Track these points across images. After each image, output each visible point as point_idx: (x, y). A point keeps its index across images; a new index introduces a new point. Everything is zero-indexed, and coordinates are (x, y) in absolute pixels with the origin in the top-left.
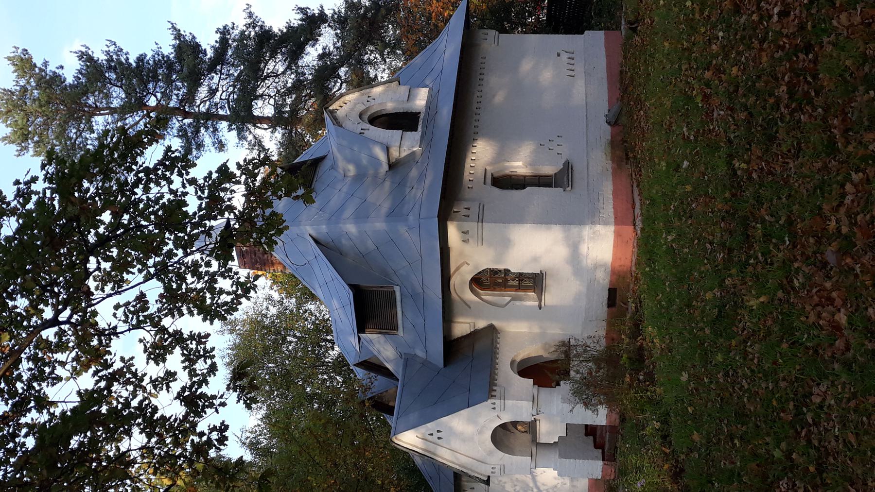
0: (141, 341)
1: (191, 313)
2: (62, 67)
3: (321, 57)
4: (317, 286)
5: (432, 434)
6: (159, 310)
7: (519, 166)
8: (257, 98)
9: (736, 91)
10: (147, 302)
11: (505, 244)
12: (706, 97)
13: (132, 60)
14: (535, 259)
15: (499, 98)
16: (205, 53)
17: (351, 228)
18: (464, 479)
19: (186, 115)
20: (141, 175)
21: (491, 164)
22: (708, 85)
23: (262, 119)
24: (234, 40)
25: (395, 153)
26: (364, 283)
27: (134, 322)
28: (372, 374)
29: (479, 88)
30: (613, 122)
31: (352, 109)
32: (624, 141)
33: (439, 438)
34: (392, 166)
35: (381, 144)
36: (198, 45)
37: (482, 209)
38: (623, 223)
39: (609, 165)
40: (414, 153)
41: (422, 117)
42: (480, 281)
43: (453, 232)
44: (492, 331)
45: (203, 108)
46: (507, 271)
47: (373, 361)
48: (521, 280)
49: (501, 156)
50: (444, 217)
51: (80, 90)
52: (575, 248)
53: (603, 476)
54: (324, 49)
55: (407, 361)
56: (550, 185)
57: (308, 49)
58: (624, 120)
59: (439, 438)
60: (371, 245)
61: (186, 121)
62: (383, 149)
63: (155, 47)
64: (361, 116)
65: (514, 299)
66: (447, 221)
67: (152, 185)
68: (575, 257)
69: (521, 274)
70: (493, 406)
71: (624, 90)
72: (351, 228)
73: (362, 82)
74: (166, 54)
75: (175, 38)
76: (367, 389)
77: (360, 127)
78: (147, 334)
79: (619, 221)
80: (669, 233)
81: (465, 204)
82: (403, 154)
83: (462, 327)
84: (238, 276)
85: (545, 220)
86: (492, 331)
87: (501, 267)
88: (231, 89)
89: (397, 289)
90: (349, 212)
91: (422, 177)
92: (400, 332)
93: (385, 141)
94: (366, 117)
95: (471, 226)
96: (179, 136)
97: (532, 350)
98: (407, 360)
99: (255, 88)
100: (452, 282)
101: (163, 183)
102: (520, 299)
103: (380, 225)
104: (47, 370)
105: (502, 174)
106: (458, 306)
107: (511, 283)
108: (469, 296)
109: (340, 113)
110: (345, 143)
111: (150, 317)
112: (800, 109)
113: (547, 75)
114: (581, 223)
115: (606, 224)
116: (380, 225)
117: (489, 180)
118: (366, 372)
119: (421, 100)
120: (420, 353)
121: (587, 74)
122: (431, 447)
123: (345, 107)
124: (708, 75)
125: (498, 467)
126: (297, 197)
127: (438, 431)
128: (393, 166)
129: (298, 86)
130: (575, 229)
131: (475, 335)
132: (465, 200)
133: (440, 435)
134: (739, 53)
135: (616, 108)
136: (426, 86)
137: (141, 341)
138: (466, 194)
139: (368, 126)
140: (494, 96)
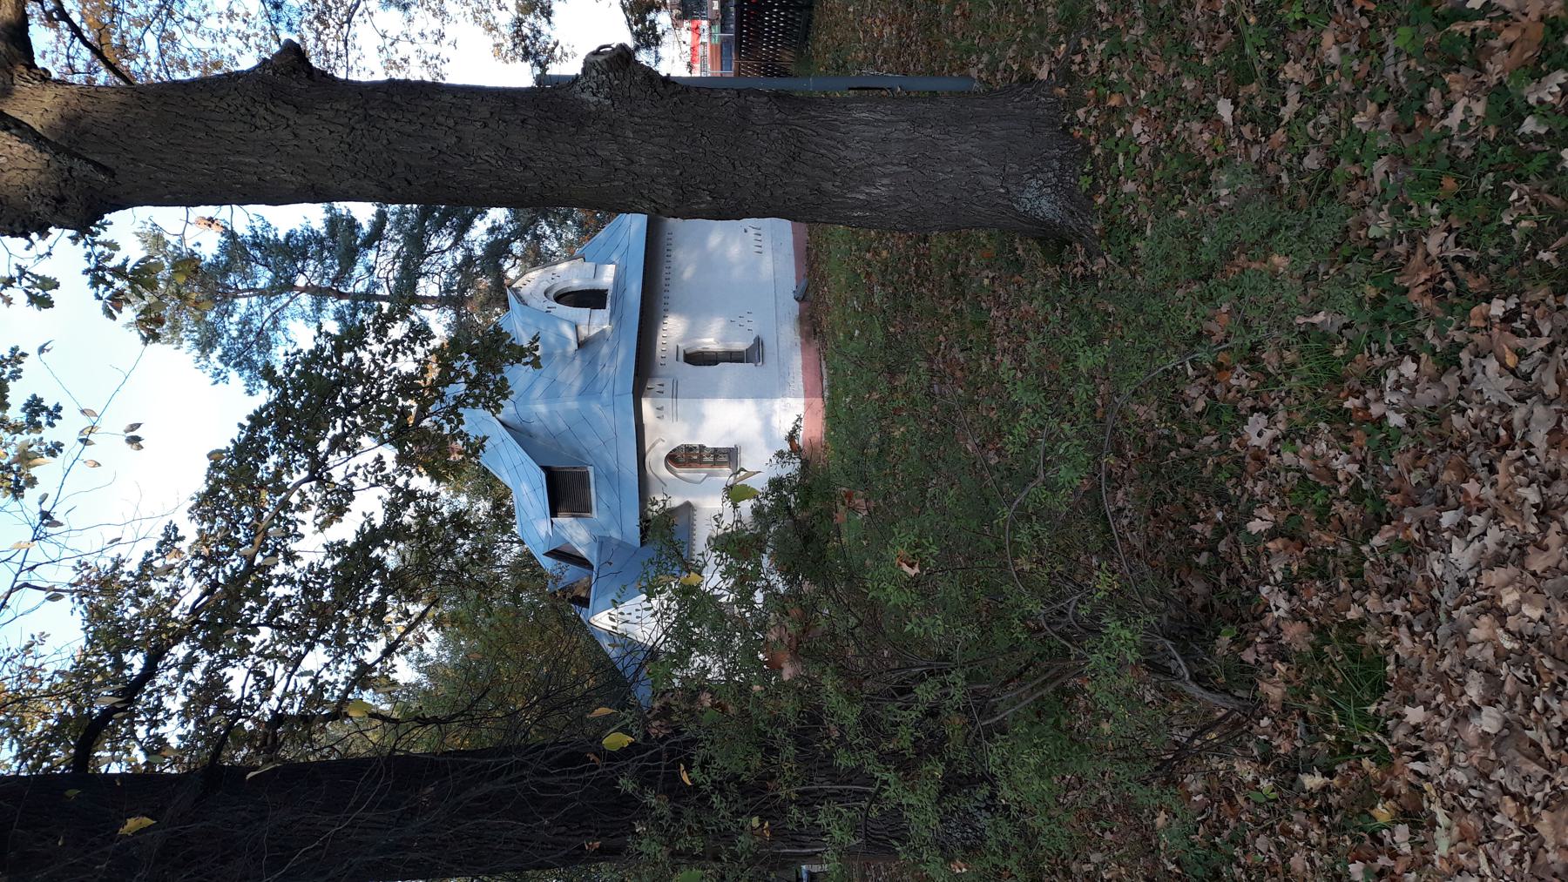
0: (380, 498)
1: (420, 475)
2: (199, 244)
3: (491, 231)
4: (503, 471)
6: (394, 471)
7: (710, 342)
8: (421, 275)
9: (886, 270)
10: (384, 463)
11: (699, 418)
12: (868, 275)
13: (282, 237)
14: (730, 433)
15: (688, 273)
16: (359, 226)
17: (541, 408)
19: (340, 296)
20: (390, 346)
21: (684, 340)
22: (869, 265)
23: (426, 300)
24: (393, 214)
25: (584, 332)
26: (554, 464)
27: (373, 481)
28: (563, 564)
29: (668, 265)
30: (801, 298)
31: (536, 287)
32: (811, 317)
35: (569, 322)
36: (353, 219)
37: (676, 384)
39: (798, 339)
40: (603, 331)
41: (609, 294)
42: (674, 459)
43: (647, 406)
44: (688, 507)
45: (361, 288)
46: (702, 447)
47: (568, 551)
48: (716, 456)
49: (692, 332)
50: (639, 392)
51: (221, 269)
54: (494, 222)
55: (601, 543)
56: (742, 361)
57: (476, 222)
58: (811, 295)
60: (562, 425)
61: (343, 302)
62: (571, 326)
63: (304, 222)
64: (546, 293)
65: (709, 475)
66: (793, 219)
67: (399, 355)
69: (716, 449)
71: (810, 266)
72: (541, 408)
73: (537, 258)
74: (315, 229)
75: (327, 212)
76: (558, 579)
77: (546, 305)
78: (384, 492)
79: (808, 394)
80: (847, 397)
81: (659, 381)
82: (593, 333)
85: (738, 394)
86: (688, 507)
87: (696, 443)
88: (390, 267)
89: (591, 470)
90: (539, 390)
91: (613, 354)
92: (595, 514)
93: (573, 319)
94: (551, 295)
95: (666, 402)
96: (336, 319)
98: (602, 543)
99: (417, 266)
101: (409, 353)
102: (717, 475)
103: (573, 404)
104: (291, 527)
105: (694, 350)
107: (706, 459)
108: (664, 472)
109: (524, 291)
110: (529, 321)
111: (387, 477)
112: (922, 284)
113: (735, 251)
114: (773, 396)
115: (796, 396)
116: (573, 404)
118: (555, 561)
119: (607, 276)
120: (615, 534)
121: (775, 250)
123: (530, 285)
124: (868, 256)
126: (527, 363)
128: (582, 344)
129: (469, 260)
130: (766, 403)
132: (661, 377)
134: (888, 239)
135: (803, 284)
136: (612, 263)
137: (380, 498)
138: (661, 371)
139: (555, 304)
140: (682, 273)
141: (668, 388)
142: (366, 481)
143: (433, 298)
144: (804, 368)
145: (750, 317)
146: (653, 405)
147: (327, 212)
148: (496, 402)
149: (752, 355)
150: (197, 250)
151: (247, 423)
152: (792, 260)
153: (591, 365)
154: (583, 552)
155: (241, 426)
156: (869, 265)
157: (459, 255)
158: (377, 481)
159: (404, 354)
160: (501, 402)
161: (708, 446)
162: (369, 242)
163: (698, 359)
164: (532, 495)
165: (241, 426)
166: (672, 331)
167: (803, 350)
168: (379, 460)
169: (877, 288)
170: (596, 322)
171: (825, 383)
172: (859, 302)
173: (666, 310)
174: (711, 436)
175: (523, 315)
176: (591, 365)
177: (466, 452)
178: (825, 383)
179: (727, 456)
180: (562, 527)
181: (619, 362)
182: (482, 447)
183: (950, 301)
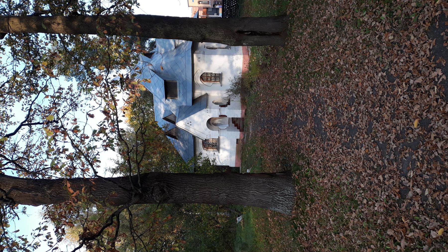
4: (151, 88)
5: (188, 123)
11: (210, 62)
18: (197, 138)
34: (176, 47)
38: (245, 55)
43: (195, 56)
44: (207, 95)
46: (211, 73)
50: (193, 53)
52: (231, 63)
53: (240, 138)
65: (213, 84)
68: (231, 66)
70: (207, 111)
83: (198, 93)
84: (51, 237)
86: (207, 95)
89: (178, 81)
95: (201, 56)
97: (219, 100)
100: (195, 77)
106: (196, 87)
115: (240, 54)
117: (206, 47)
122: (188, 128)
125: (208, 135)
130: (231, 57)
131: (201, 97)
133: (191, 123)
146: (197, 56)
174: (214, 69)
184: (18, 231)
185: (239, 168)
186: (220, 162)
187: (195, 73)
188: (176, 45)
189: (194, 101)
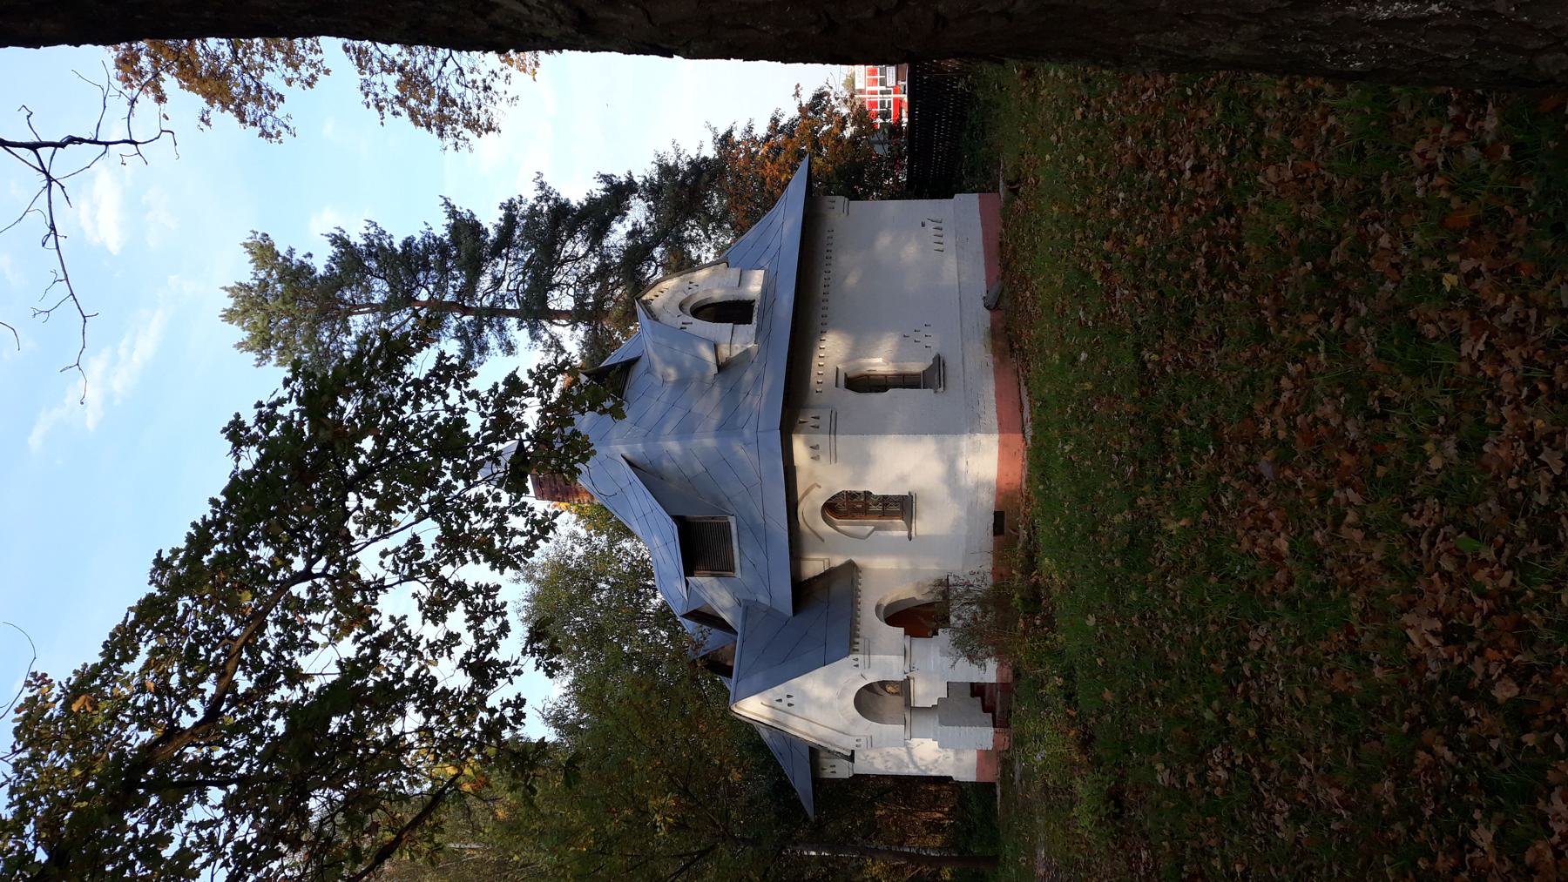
0: (415, 596)
2: (310, 255)
3: (631, 235)
6: (437, 557)
7: (879, 363)
8: (552, 287)
9: (1143, 265)
11: (864, 461)
14: (903, 479)
15: (852, 280)
16: (486, 232)
17: (673, 446)
18: (822, 754)
19: (465, 311)
20: (409, 389)
23: (560, 314)
24: (523, 217)
25: (725, 352)
26: (692, 514)
27: (406, 572)
29: (827, 268)
30: (993, 306)
31: (671, 299)
32: (1007, 329)
33: (790, 705)
36: (478, 225)
37: (834, 417)
40: (747, 351)
41: (756, 305)
44: (851, 567)
46: (868, 494)
50: (788, 428)
51: (333, 283)
54: (634, 225)
56: (918, 387)
57: (615, 225)
58: (1006, 302)
59: (790, 705)
60: (699, 468)
61: (466, 319)
62: (710, 347)
63: (424, 228)
64: (681, 306)
65: (877, 528)
71: (1006, 266)
72: (673, 446)
76: (699, 646)
77: (680, 321)
80: (1066, 442)
82: (736, 352)
83: (814, 565)
85: (916, 428)
87: (860, 489)
89: (732, 520)
91: (758, 380)
94: (688, 308)
95: (821, 439)
96: (457, 338)
98: (748, 608)
99: (550, 275)
101: (437, 398)
105: (857, 373)
107: (873, 508)
108: (824, 528)
110: (663, 341)
111: (426, 565)
112: (1221, 285)
114: (958, 431)
115: (988, 432)
116: (709, 442)
119: (755, 286)
120: (763, 599)
122: (781, 716)
123: (662, 296)
124: (1107, 246)
125: (863, 739)
127: (789, 696)
128: (722, 367)
130: (950, 440)
131: (830, 574)
132: (812, 407)
133: (790, 700)
134: (1144, 218)
135: (996, 288)
137: (415, 596)
138: (814, 398)
139: (691, 319)
140: (845, 278)
141: (825, 418)
142: (395, 572)
143: (567, 311)
144: (998, 395)
145: (927, 331)
146: (807, 443)
147: (450, 217)
148: (571, 466)
149: (932, 378)
150: (308, 261)
151: (222, 499)
152: (981, 260)
153: (732, 394)
154: (726, 617)
155: (214, 502)
156: (1108, 258)
157: (593, 264)
158: (412, 572)
159: (431, 400)
160: (579, 466)
161: (874, 493)
162: (497, 249)
163: (862, 384)
164: (663, 550)
165: (214, 502)
166: (831, 352)
167: (997, 371)
168: (415, 541)
169: (1122, 293)
170: (738, 340)
171: (1027, 415)
172: (1087, 313)
173: (823, 328)
174: (879, 483)
175: (653, 333)
176: (732, 394)
177: (530, 533)
178: (1027, 415)
179: (901, 507)
180: (700, 587)
181: (766, 395)
182: (553, 527)
183: (1312, 318)
184: (167, 119)
185: (993, 785)
186: (916, 766)
187: (800, 492)
188: (722, 360)
189: (803, 591)
